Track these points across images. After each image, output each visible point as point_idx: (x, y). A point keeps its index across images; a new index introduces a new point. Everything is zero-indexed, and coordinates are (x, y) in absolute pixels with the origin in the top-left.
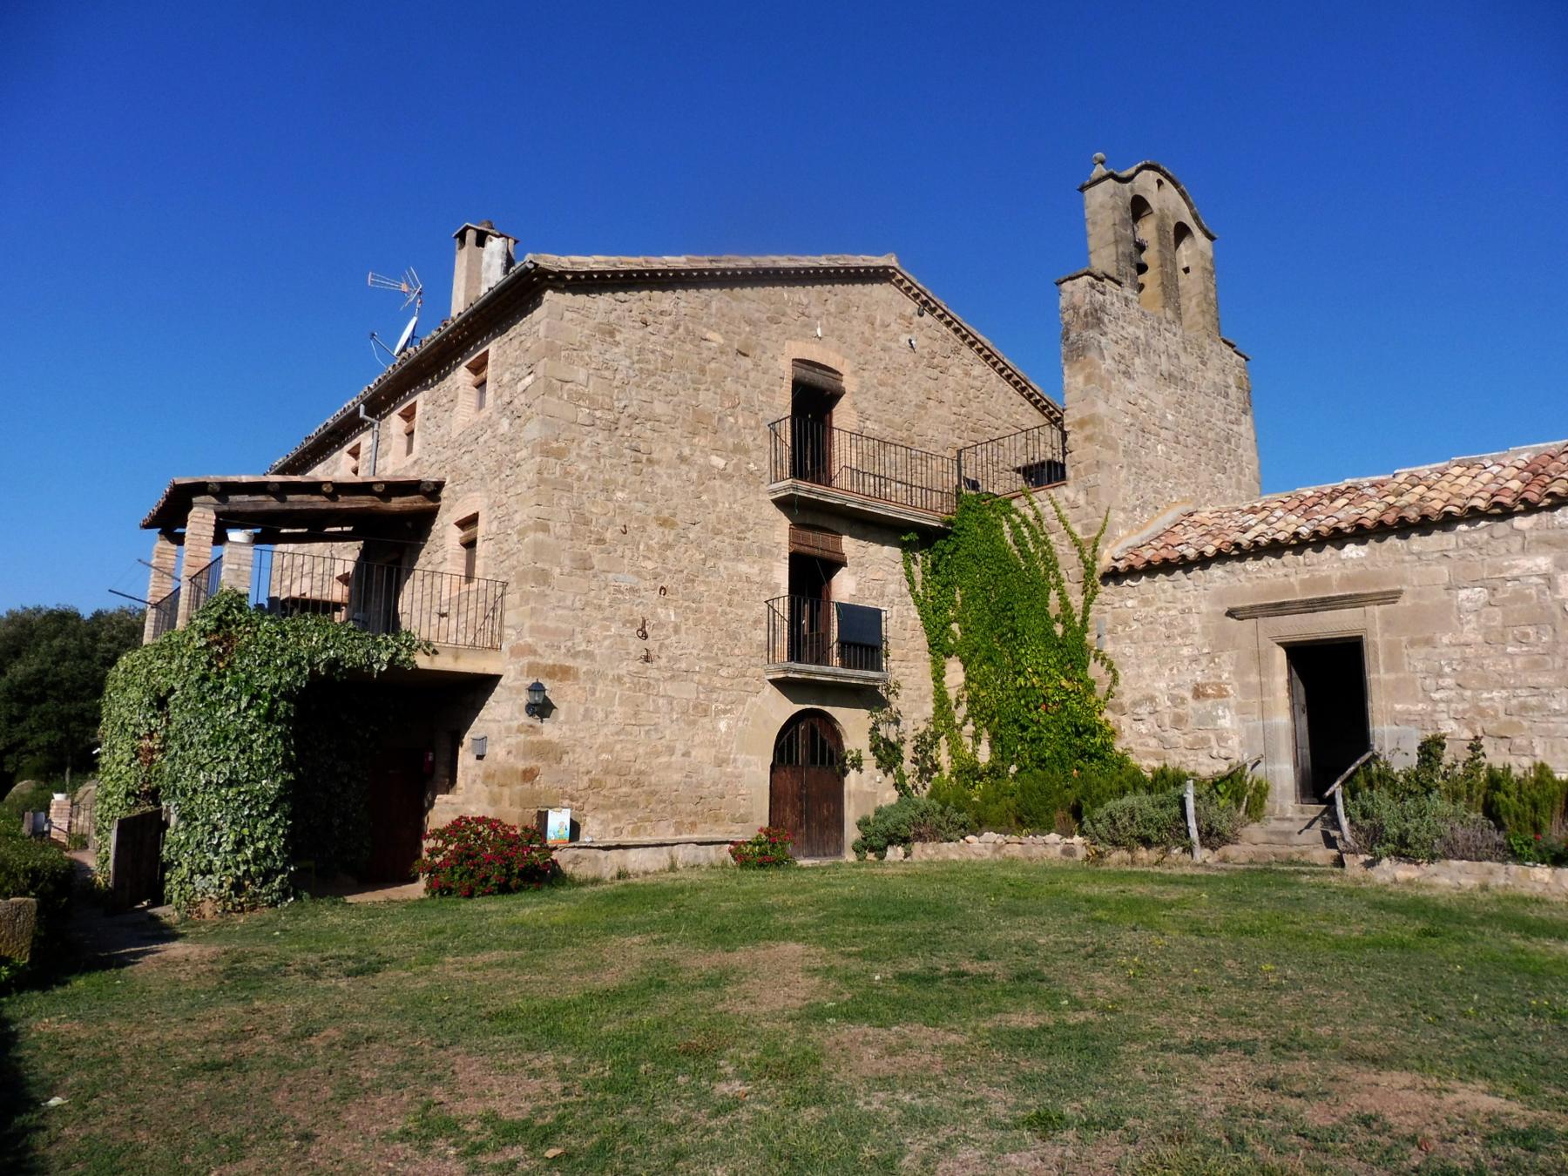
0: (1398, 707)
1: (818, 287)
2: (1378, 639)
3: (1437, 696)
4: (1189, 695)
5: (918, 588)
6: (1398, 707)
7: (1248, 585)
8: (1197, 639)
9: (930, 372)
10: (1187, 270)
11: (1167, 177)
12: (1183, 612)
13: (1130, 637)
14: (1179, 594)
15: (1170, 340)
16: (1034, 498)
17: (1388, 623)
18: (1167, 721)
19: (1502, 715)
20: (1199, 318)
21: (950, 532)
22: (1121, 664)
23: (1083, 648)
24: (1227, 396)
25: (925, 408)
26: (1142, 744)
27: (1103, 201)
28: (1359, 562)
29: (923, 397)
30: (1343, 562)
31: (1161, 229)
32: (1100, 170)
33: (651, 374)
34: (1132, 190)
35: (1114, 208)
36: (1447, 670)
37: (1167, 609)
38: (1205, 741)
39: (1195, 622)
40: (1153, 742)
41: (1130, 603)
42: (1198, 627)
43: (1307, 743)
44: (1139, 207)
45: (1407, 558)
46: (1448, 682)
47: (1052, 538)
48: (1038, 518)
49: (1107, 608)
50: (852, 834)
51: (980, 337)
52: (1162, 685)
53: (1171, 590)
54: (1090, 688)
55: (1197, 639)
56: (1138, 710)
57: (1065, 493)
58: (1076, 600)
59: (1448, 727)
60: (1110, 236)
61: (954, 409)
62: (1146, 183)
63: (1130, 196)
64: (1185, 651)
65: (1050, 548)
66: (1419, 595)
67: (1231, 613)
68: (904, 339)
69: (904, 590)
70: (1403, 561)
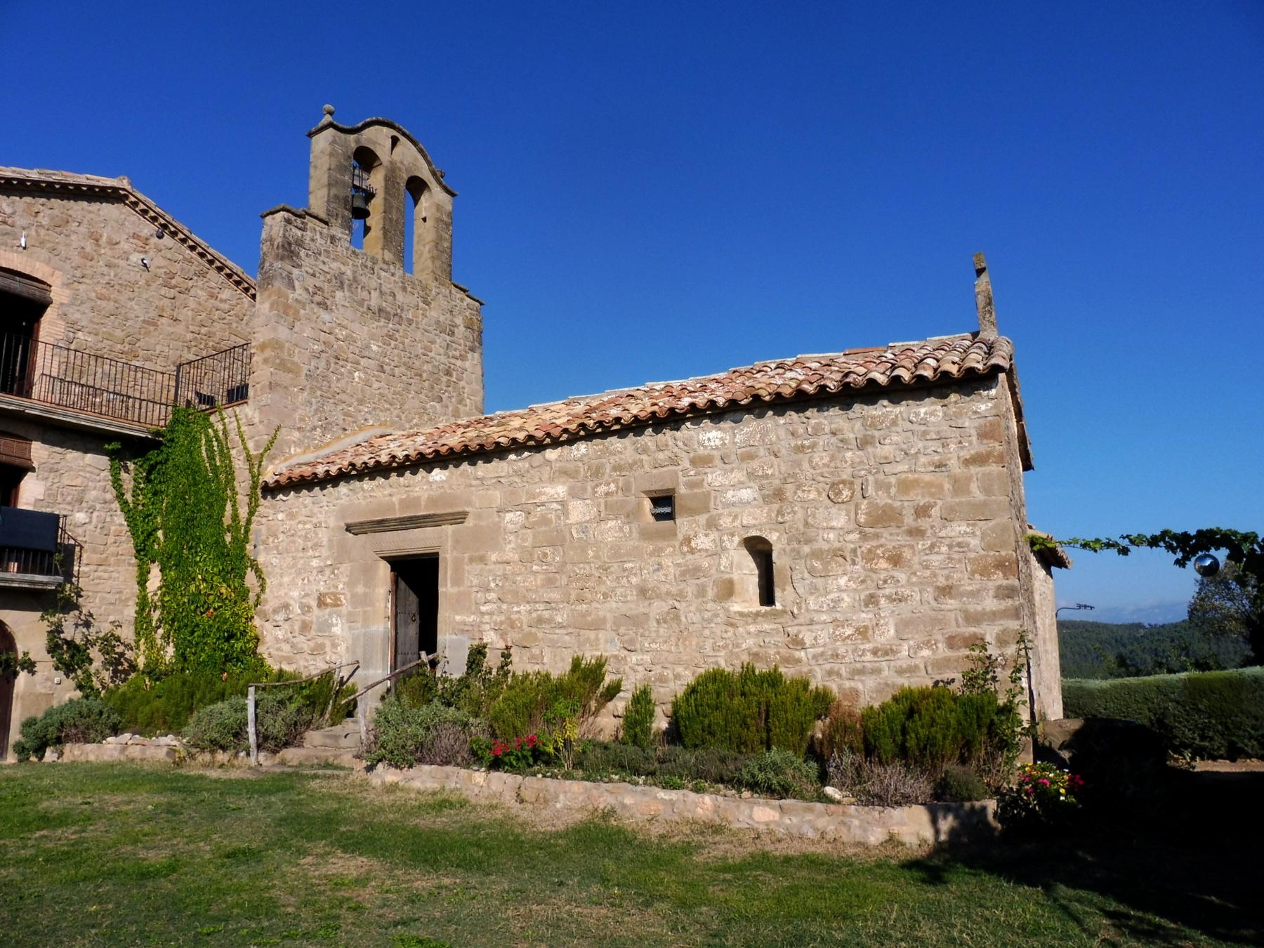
0: (458, 618)
1: (28, 199)
3: (483, 609)
4: (314, 604)
5: (128, 497)
6: (458, 618)
9: (163, 291)
10: (424, 220)
11: (404, 134)
13: (277, 548)
14: (316, 510)
15: (390, 278)
17: (457, 542)
18: (297, 628)
19: (525, 627)
20: (429, 263)
21: (161, 443)
22: (269, 573)
23: (242, 557)
24: (452, 334)
25: (155, 325)
26: (278, 649)
28: (441, 485)
29: (153, 314)
30: (430, 483)
31: (390, 180)
32: (327, 119)
34: (357, 141)
35: (331, 155)
36: (493, 585)
37: (305, 523)
38: (322, 646)
39: (324, 536)
40: (286, 647)
41: (280, 516)
42: (325, 541)
44: (366, 159)
45: (474, 482)
46: (492, 596)
47: (233, 452)
49: (264, 520)
50: (15, 735)
52: (295, 594)
54: (243, 594)
55: (325, 552)
57: (247, 411)
58: (243, 512)
59: (490, 637)
60: (325, 180)
61: (191, 328)
63: (354, 146)
64: (315, 563)
67: (349, 528)
68: (135, 258)
69: (109, 496)
70: (471, 486)
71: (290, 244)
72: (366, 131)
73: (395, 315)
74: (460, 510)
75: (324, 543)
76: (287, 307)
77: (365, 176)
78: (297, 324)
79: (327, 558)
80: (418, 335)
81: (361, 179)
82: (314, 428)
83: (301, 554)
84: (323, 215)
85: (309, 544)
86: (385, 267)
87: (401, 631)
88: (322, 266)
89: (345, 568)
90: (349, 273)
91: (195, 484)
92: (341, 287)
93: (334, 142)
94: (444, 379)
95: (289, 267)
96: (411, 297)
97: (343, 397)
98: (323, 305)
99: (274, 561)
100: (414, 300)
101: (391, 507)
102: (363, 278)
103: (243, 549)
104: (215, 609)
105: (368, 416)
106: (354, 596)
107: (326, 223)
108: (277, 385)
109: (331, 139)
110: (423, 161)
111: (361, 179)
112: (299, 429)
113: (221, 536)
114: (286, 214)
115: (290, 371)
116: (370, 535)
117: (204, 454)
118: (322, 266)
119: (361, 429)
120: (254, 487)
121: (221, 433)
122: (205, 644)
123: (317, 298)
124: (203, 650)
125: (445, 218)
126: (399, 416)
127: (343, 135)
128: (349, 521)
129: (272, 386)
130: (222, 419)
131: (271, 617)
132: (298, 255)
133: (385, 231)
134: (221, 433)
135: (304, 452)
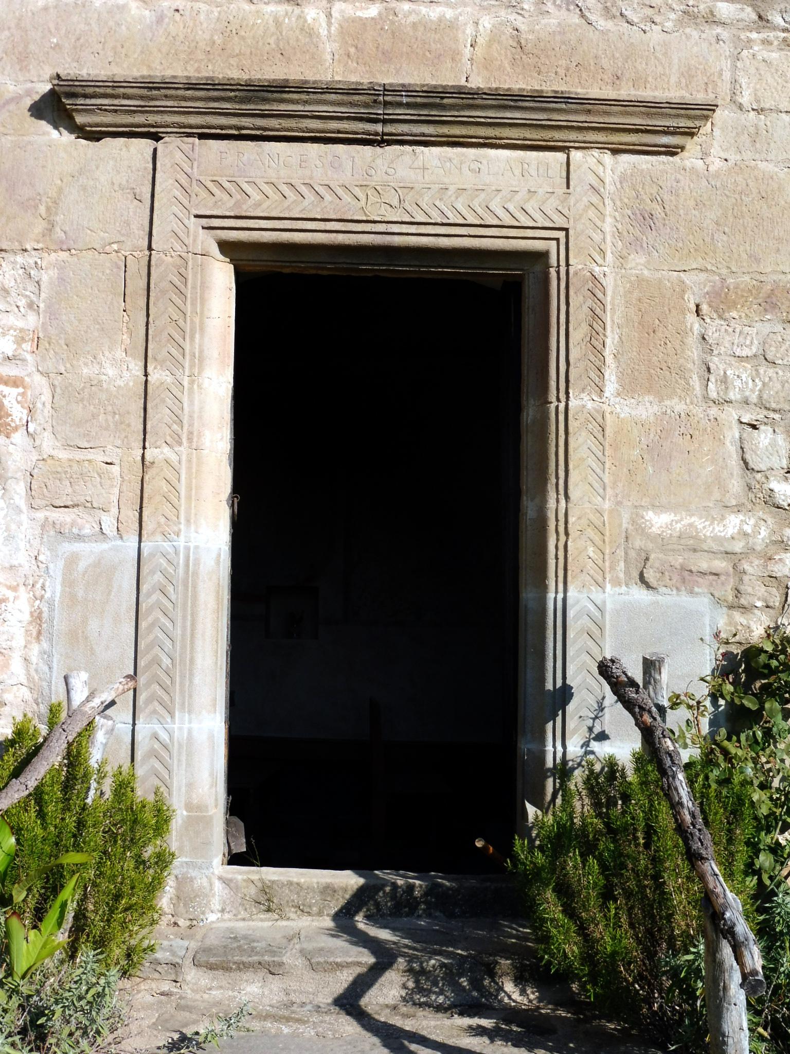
0: (659, 521)
17: (644, 221)
33: (560, 32)
67: (58, 106)
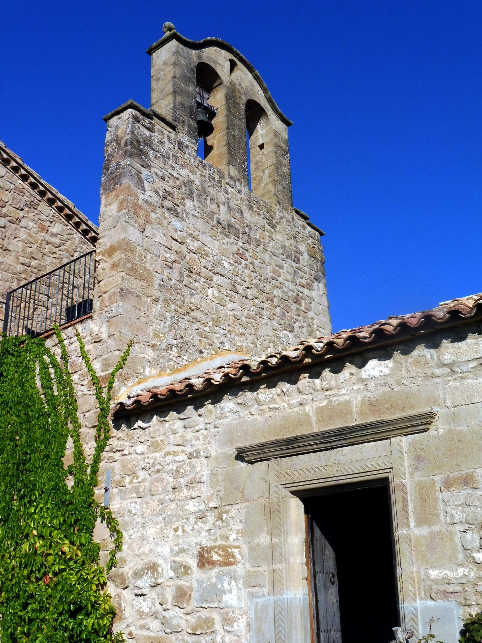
0: (434, 574)
2: (407, 481)
4: (193, 562)
6: (434, 574)
7: (260, 419)
8: (205, 490)
10: (262, 147)
11: (241, 60)
12: (191, 456)
13: (136, 490)
15: (237, 195)
16: (64, 336)
17: (418, 459)
18: (169, 596)
20: (271, 187)
22: (127, 524)
23: (90, 504)
24: (297, 260)
26: (143, 627)
27: (167, 61)
31: (231, 98)
32: (168, 33)
37: (175, 454)
38: (209, 622)
39: (203, 468)
40: (155, 625)
41: (140, 448)
42: (205, 475)
43: (337, 623)
44: (206, 77)
45: (438, 371)
47: (75, 377)
48: (65, 357)
49: (117, 455)
51: (60, 195)
52: (165, 550)
53: (181, 430)
54: (92, 554)
55: (205, 490)
56: (140, 583)
57: (92, 327)
60: (170, 88)
61: (22, 259)
62: (218, 58)
63: (196, 61)
64: (192, 506)
65: (72, 389)
66: (454, 418)
70: (434, 376)
71: (138, 142)
72: (207, 50)
73: (244, 233)
74: (426, 410)
75: (205, 478)
76: (137, 208)
77: (206, 95)
78: (148, 227)
79: (210, 498)
80: (267, 257)
81: (202, 97)
82: (170, 347)
83: (172, 496)
84: (169, 118)
85: (183, 481)
86: (232, 182)
87: (321, 598)
88: (171, 171)
89: (236, 511)
90: (197, 182)
91: (28, 421)
92: (191, 195)
93: (176, 53)
94: (294, 307)
95: (138, 166)
96: (257, 217)
97: (198, 315)
98: (172, 211)
99: (134, 508)
100: (260, 220)
101: (305, 420)
102: (211, 189)
103: (90, 494)
104: (55, 574)
105: (224, 339)
106: (254, 549)
107: (174, 128)
108: (130, 292)
109: (174, 49)
110: (259, 88)
111: (202, 97)
112: (153, 346)
113: (61, 479)
114: (134, 112)
115: (142, 278)
116: (273, 463)
117: (38, 384)
118: (171, 171)
119: (217, 354)
120: (104, 411)
121: (59, 359)
122: (43, 620)
123: (167, 204)
124: (39, 629)
125: (282, 144)
126: (254, 343)
127: (185, 49)
128: (240, 445)
129: (123, 293)
130: (61, 342)
131: (131, 582)
132: (146, 155)
133: (230, 148)
134: (59, 359)
135: (160, 375)
